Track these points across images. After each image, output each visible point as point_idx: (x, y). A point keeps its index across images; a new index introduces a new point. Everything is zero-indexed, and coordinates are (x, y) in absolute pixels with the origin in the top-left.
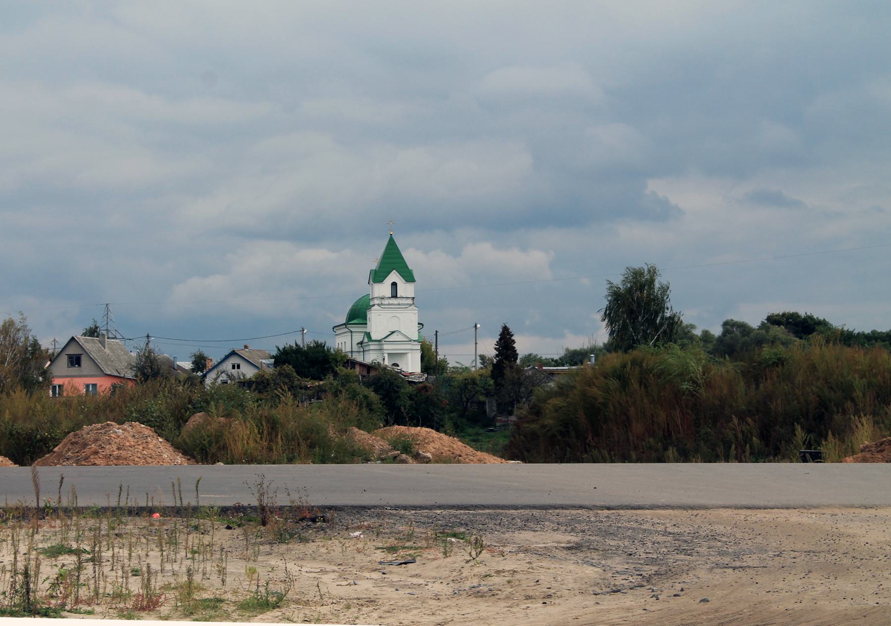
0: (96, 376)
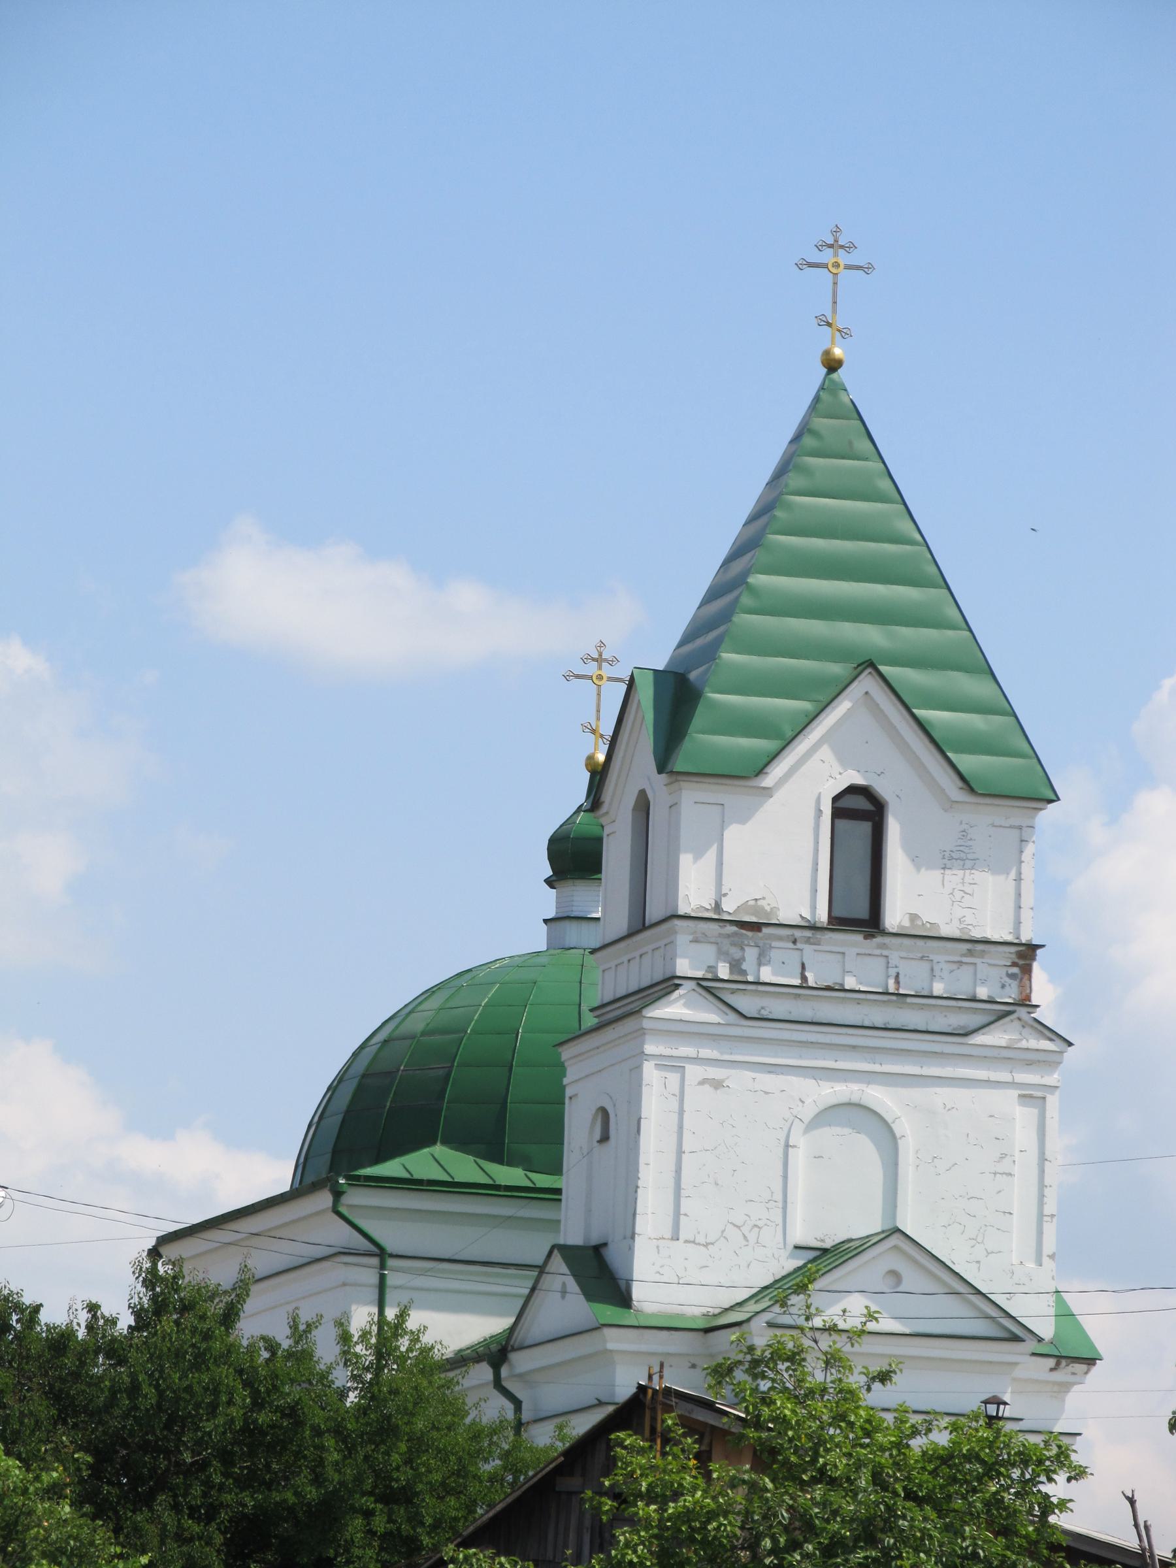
0: (397, 1027)
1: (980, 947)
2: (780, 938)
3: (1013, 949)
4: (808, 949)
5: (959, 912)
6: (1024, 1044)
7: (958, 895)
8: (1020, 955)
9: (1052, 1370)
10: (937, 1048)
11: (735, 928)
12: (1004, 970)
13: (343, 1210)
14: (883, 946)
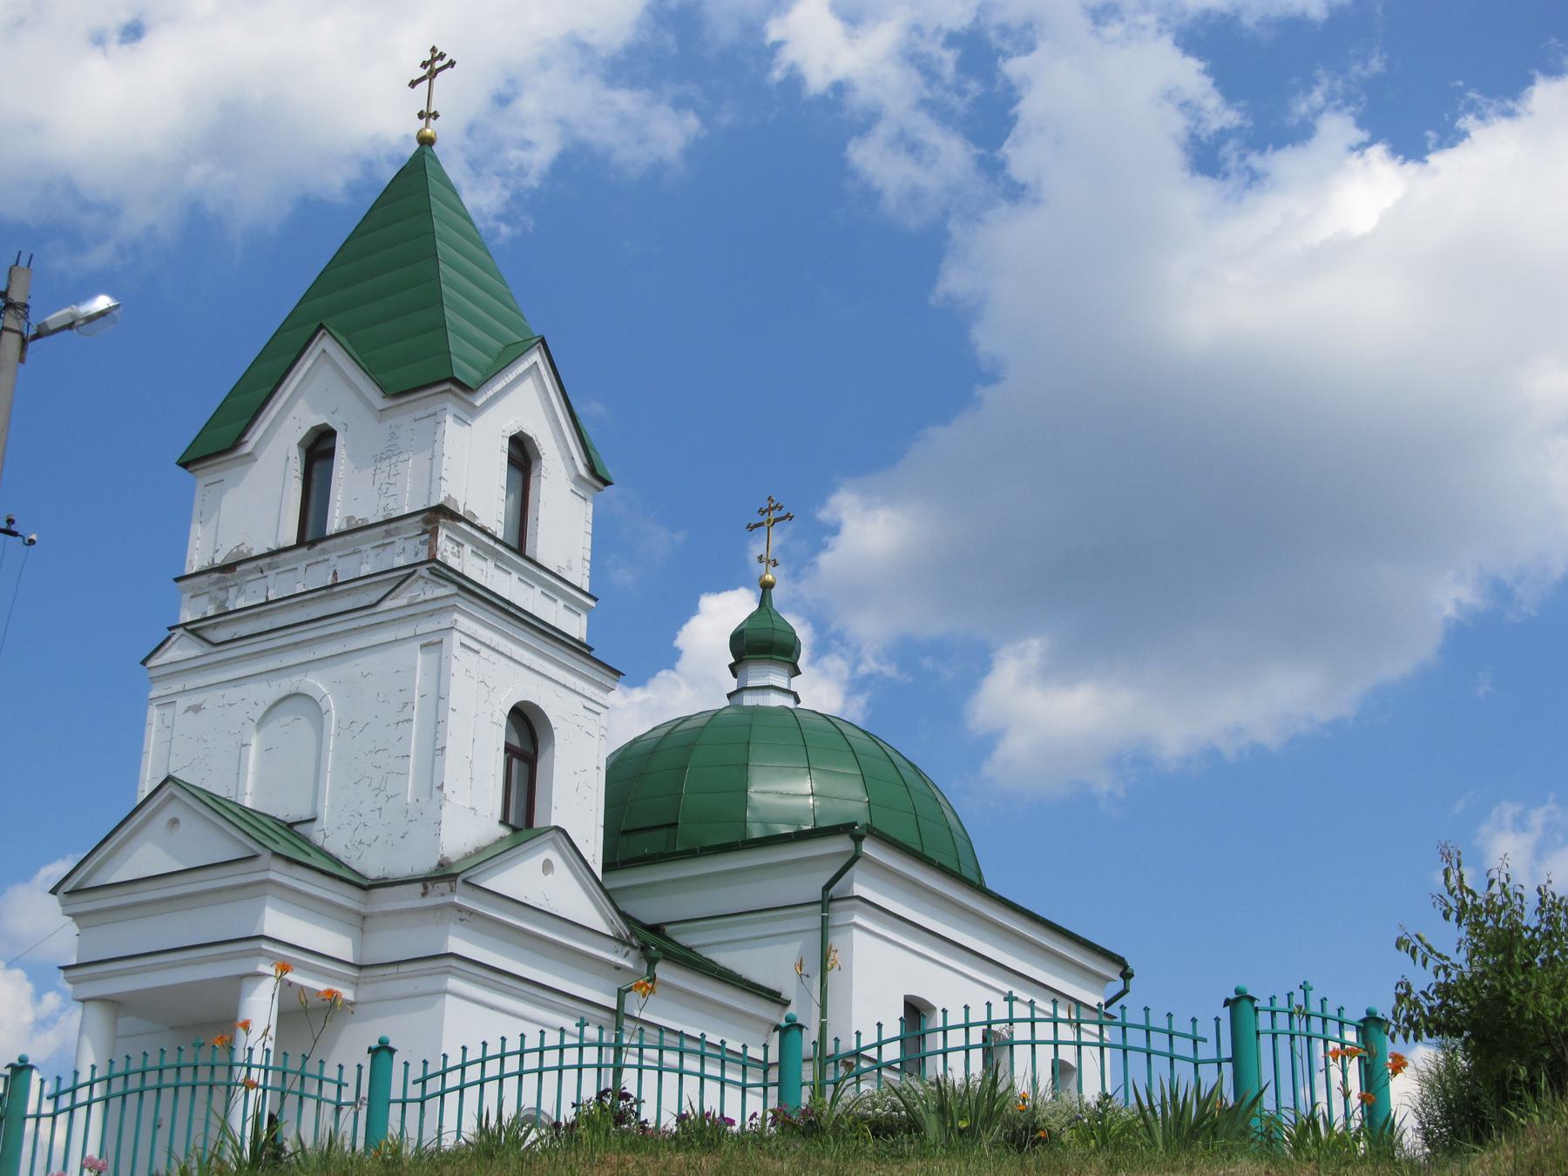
1: (393, 526)
2: (251, 572)
3: (418, 518)
4: (271, 574)
5: (384, 502)
6: (429, 596)
7: (384, 488)
8: (427, 521)
9: (424, 895)
10: (355, 624)
11: (216, 575)
12: (417, 540)
13: (1113, 972)
14: (323, 552)
